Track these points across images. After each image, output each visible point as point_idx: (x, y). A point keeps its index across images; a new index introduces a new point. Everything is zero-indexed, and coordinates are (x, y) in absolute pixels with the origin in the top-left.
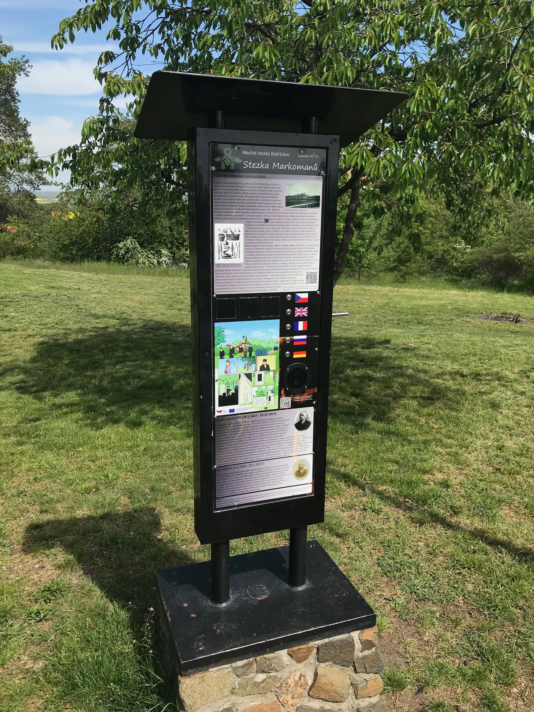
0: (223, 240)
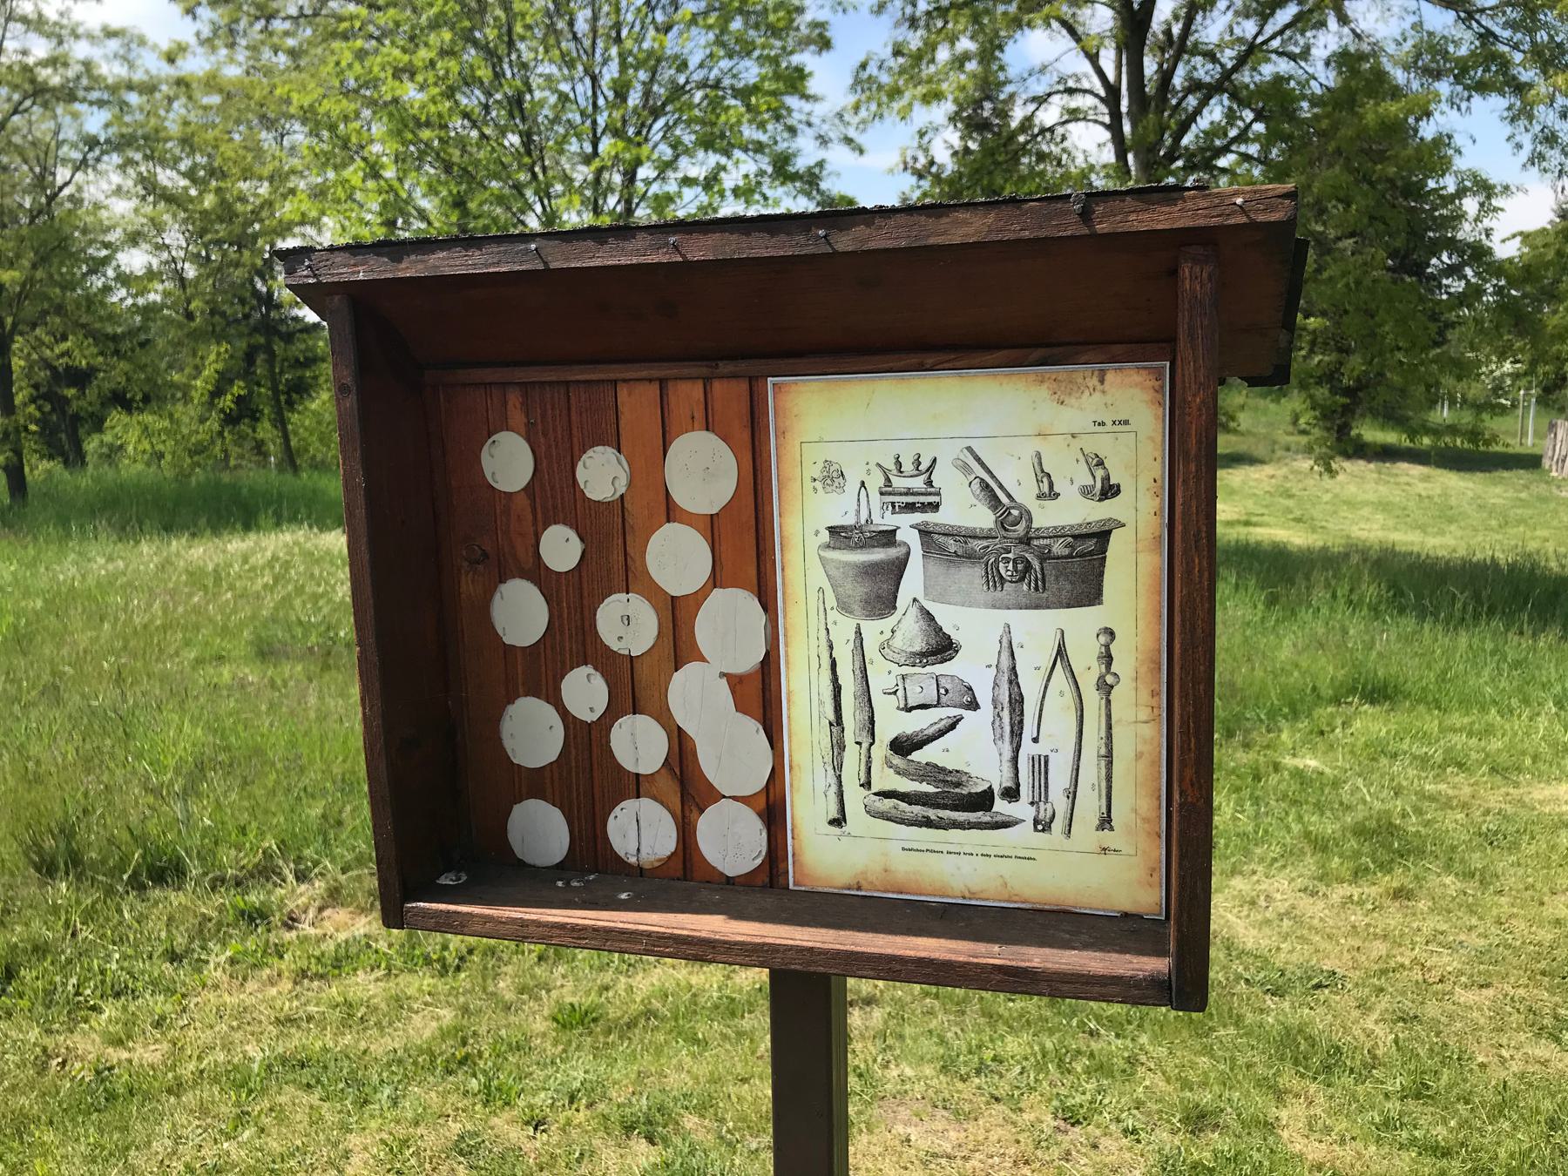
0: (883, 603)
